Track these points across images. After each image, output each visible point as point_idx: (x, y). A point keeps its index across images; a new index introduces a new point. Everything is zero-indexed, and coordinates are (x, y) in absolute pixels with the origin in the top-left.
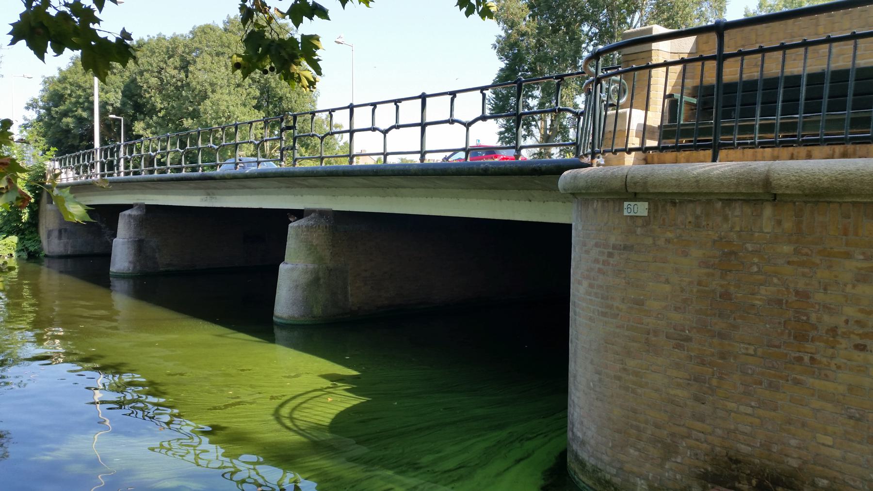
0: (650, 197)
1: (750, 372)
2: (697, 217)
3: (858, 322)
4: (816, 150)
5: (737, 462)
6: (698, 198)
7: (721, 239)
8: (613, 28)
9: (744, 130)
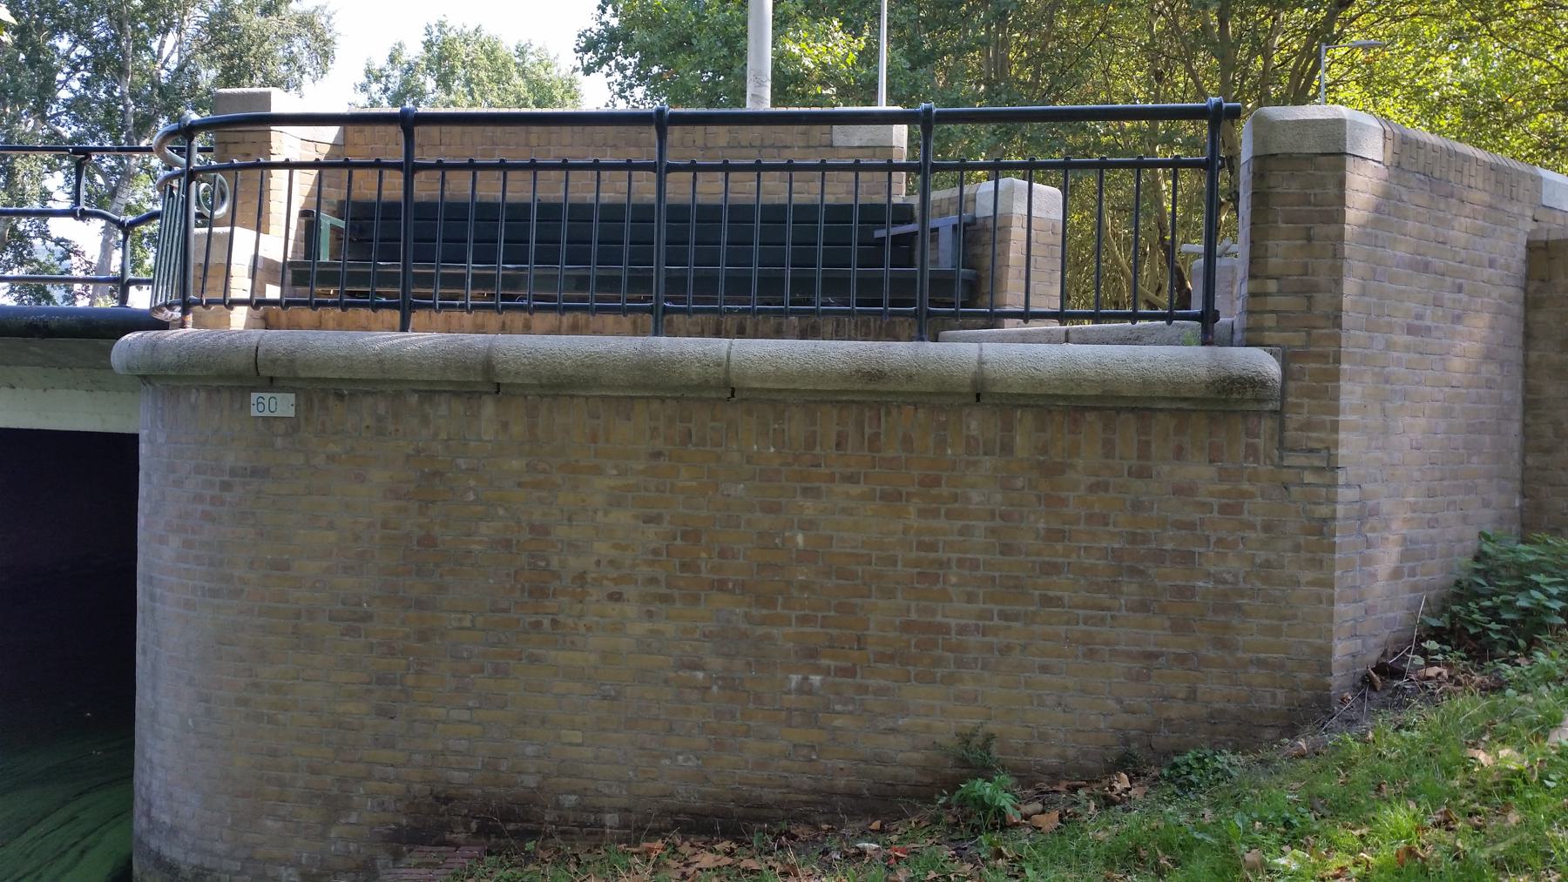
0: (298, 384)
1: (465, 654)
2: (380, 419)
3: (612, 563)
4: (539, 319)
5: (448, 800)
6: (379, 388)
7: (419, 452)
8: (124, 54)
9: (449, 281)
